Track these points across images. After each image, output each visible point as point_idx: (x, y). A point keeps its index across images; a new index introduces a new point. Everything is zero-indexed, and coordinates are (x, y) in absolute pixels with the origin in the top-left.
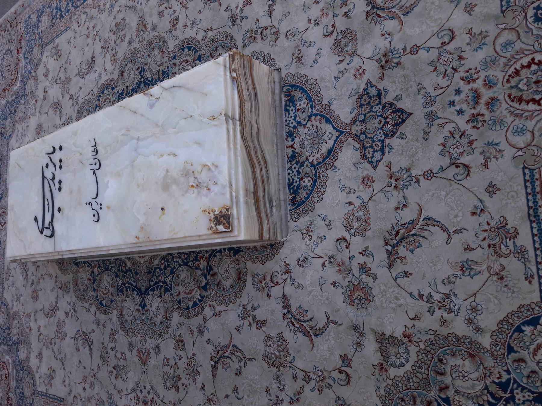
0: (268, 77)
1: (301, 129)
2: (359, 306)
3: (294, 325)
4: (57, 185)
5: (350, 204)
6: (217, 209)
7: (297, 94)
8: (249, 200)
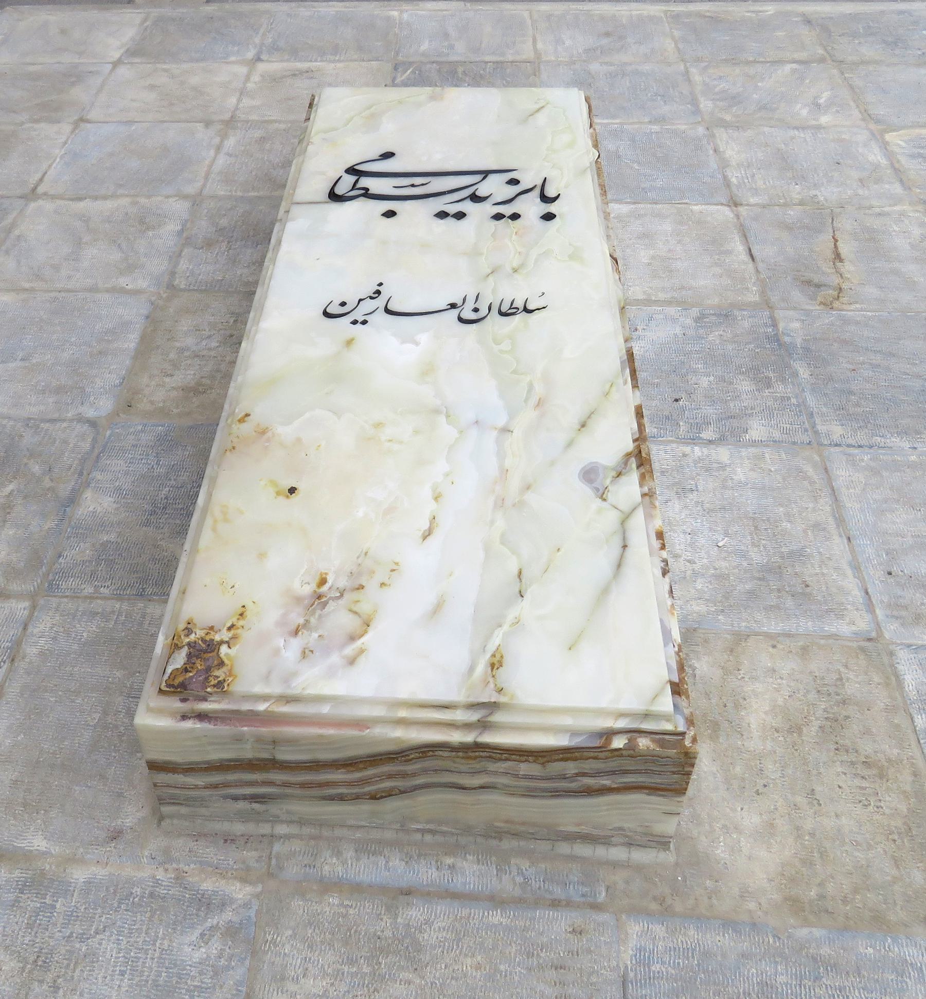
0: (639, 829)
4: (453, 209)
6: (232, 652)
8: (248, 746)
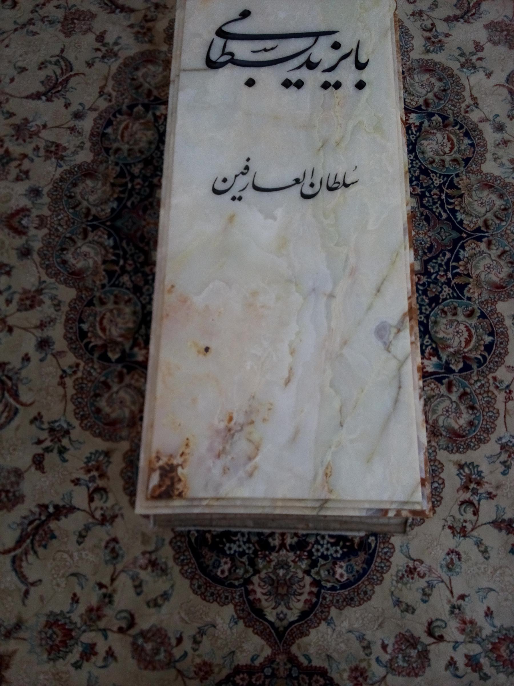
1: (304, 565)
2: (43, 636)
3: (474, 14)
4: (294, 77)
5: (180, 640)
7: (358, 562)
